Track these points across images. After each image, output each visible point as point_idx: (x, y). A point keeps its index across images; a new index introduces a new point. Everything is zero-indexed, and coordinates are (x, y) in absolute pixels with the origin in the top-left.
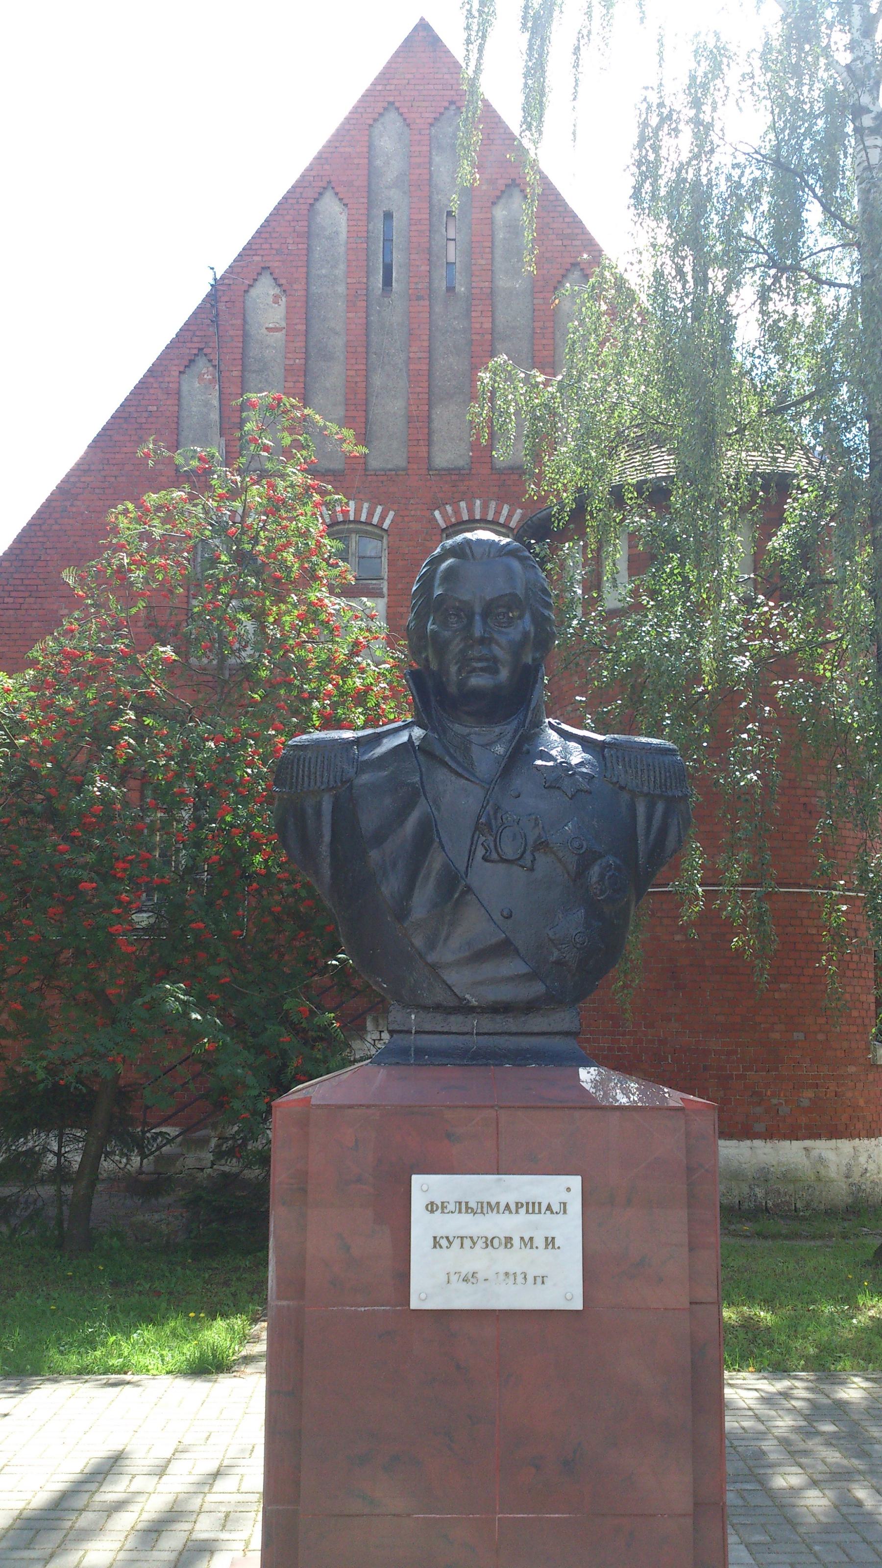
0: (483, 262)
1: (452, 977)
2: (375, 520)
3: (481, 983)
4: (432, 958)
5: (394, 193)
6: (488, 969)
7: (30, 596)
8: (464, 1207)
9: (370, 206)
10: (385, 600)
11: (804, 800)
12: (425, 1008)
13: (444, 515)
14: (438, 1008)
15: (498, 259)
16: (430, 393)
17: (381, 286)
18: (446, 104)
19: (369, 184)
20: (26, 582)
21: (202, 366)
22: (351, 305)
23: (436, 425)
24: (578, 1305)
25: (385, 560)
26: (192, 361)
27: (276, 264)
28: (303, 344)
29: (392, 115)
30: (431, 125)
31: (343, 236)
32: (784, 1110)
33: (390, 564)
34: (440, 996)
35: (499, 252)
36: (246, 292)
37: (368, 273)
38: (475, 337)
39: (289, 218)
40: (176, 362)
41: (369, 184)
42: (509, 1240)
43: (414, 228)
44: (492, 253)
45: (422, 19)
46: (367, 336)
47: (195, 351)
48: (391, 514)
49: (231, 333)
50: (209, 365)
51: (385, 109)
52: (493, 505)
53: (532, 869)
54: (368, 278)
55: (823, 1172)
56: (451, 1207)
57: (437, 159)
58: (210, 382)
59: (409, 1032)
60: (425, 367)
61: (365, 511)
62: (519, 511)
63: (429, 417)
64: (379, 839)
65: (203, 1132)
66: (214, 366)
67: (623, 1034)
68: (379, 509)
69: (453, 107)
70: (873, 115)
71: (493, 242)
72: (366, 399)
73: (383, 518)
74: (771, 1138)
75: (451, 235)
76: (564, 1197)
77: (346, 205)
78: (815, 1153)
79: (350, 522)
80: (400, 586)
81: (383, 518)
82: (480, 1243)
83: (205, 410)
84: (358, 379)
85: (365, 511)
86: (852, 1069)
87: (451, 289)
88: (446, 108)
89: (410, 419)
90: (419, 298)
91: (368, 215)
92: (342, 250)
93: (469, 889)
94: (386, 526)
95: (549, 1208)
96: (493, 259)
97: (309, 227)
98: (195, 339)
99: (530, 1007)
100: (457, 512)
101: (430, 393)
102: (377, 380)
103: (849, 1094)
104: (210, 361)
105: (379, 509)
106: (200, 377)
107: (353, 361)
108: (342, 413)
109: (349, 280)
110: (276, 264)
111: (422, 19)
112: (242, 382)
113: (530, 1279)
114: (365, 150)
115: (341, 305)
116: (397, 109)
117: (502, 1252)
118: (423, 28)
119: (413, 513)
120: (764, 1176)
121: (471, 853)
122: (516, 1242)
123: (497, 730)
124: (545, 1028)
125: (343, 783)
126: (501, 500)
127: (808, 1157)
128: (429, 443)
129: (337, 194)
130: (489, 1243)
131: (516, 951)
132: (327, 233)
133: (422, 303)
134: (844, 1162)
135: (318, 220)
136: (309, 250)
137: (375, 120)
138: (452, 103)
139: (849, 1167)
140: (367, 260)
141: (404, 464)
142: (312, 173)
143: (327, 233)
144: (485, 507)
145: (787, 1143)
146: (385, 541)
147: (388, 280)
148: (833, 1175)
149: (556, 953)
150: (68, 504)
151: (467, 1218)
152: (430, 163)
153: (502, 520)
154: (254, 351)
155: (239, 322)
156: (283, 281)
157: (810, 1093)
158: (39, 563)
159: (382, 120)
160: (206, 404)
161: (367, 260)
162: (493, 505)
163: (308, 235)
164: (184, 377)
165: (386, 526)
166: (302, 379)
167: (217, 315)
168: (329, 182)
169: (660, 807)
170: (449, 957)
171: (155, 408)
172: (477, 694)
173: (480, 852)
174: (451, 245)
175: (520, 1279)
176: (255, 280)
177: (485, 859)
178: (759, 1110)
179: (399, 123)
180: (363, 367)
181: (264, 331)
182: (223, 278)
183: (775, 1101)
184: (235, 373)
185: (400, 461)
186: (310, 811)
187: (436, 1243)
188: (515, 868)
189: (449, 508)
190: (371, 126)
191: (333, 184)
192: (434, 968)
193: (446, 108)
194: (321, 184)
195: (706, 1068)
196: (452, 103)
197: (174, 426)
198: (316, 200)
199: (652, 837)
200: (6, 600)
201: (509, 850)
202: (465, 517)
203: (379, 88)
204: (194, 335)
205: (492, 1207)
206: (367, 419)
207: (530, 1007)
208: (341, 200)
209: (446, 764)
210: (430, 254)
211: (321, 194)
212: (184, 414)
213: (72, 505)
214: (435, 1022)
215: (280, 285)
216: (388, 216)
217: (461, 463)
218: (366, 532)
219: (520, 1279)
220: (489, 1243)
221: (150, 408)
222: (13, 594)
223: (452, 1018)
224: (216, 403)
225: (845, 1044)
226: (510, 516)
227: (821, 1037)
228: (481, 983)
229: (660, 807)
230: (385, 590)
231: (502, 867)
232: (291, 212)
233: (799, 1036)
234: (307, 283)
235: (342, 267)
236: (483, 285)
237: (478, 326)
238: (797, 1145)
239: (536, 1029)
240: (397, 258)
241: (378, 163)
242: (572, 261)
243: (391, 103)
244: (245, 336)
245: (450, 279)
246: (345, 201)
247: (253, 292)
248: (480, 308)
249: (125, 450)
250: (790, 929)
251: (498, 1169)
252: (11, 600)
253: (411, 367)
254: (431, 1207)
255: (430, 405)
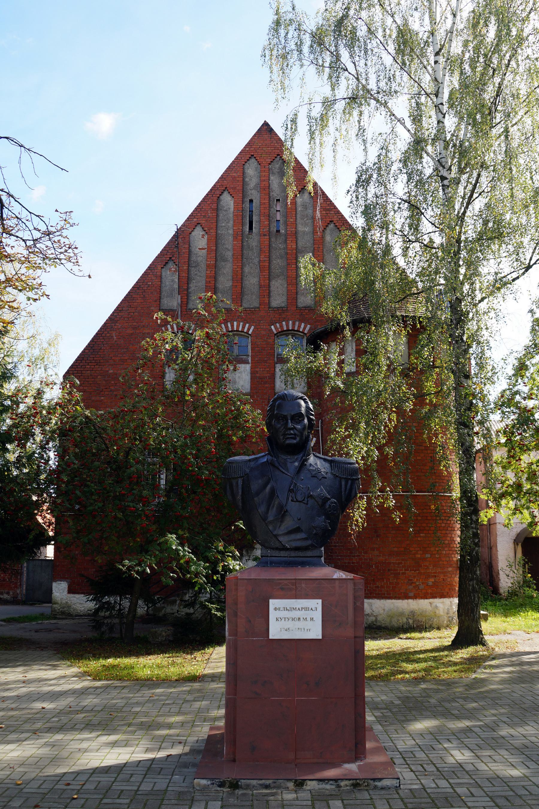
0: (292, 220)
1: (281, 539)
2: (245, 330)
3: (291, 541)
4: (275, 533)
5: (254, 192)
6: (293, 536)
7: (97, 365)
8: (286, 609)
9: (243, 197)
10: (250, 365)
11: (431, 455)
12: (273, 549)
13: (276, 328)
14: (277, 549)
15: (298, 219)
16: (269, 275)
17: (248, 230)
18: (276, 156)
19: (243, 189)
20: (95, 359)
21: (171, 265)
22: (235, 238)
23: (272, 288)
24: (320, 637)
25: (250, 347)
26: (166, 263)
27: (203, 222)
28: (214, 255)
29: (253, 160)
30: (269, 164)
31: (232, 210)
32: (422, 587)
33: (252, 349)
34: (278, 545)
35: (298, 216)
36: (190, 233)
37: (243, 225)
38: (288, 251)
39: (209, 202)
40: (160, 263)
41: (243, 189)
42: (299, 619)
43: (262, 206)
44: (296, 216)
45: (265, 121)
46: (242, 251)
47: (168, 259)
48: (253, 327)
49: (184, 251)
50: (174, 264)
51: (250, 158)
52: (297, 323)
53: (307, 504)
54: (242, 227)
55: (437, 612)
56: (282, 609)
57: (272, 178)
58: (174, 271)
59: (268, 556)
60: (267, 264)
61: (241, 326)
62: (309, 326)
63: (269, 285)
64: (258, 494)
65: (173, 598)
66: (176, 265)
67: (354, 556)
68: (247, 325)
69: (279, 157)
70: (448, 180)
71: (296, 212)
72: (242, 278)
73: (249, 329)
74: (416, 599)
75: (278, 209)
76: (317, 606)
77: (233, 197)
78: (434, 605)
79: (235, 331)
80: (256, 359)
81: (249, 329)
82: (291, 620)
83: (172, 283)
84: (238, 270)
85: (241, 326)
86: (450, 569)
87: (278, 231)
88: (276, 157)
89: (260, 286)
90: (265, 235)
91: (243, 201)
92: (231, 215)
93: (287, 511)
94: (250, 332)
95: (312, 609)
96: (296, 219)
97: (217, 206)
98: (168, 254)
99: (306, 548)
100: (281, 326)
101: (269, 275)
102: (247, 269)
103: (449, 580)
104: (175, 263)
105: (247, 325)
106: (170, 270)
107: (236, 262)
108: (231, 284)
109: (234, 228)
110: (203, 222)
111: (265, 121)
112: (188, 271)
113: (306, 630)
114: (242, 174)
115: (231, 238)
116: (255, 157)
117: (297, 622)
118: (266, 125)
119: (262, 327)
120: (413, 613)
121: (288, 499)
122: (302, 619)
123: (296, 457)
124: (311, 555)
125: (245, 475)
126: (301, 321)
127: (431, 606)
128: (269, 296)
129: (229, 192)
130: (293, 619)
131: (302, 531)
132: (225, 209)
133: (266, 237)
134: (446, 608)
135: (221, 203)
136: (217, 216)
137: (246, 162)
138: (278, 155)
139: (448, 610)
140: (242, 220)
141: (258, 305)
142: (219, 184)
143: (225, 209)
144: (294, 324)
145: (423, 600)
146: (250, 339)
147: (251, 228)
148: (442, 613)
149: (315, 531)
150: (113, 324)
151: (286, 612)
152: (269, 180)
153: (301, 330)
154: (193, 258)
155: (187, 246)
156: (206, 229)
157: (432, 580)
158: (101, 351)
159: (248, 162)
160: (173, 281)
161: (242, 220)
162: (297, 323)
163: (217, 210)
164: (164, 269)
165: (250, 332)
166: (214, 270)
167: (178, 244)
168: (226, 188)
169: (350, 482)
170: (281, 533)
171: (151, 283)
172: (290, 445)
173: (290, 499)
174: (278, 213)
175: (303, 630)
176: (194, 229)
177: (292, 501)
178: (411, 587)
179: (256, 163)
180: (241, 264)
181: (198, 250)
182: (180, 228)
183: (417, 583)
184: (185, 268)
185: (256, 304)
186: (234, 484)
187: (277, 620)
188: (302, 504)
189: (278, 325)
190: (244, 165)
191: (228, 189)
192: (276, 536)
193: (276, 157)
194: (223, 189)
195: (389, 570)
196: (278, 155)
197: (159, 290)
198: (220, 195)
199: (347, 492)
200: (87, 366)
201: (299, 499)
202: (285, 329)
203: (247, 149)
204: (168, 252)
205: (295, 609)
206: (242, 286)
207: (306, 548)
208: (231, 195)
209: (279, 469)
210: (269, 217)
211: (222, 193)
212: (163, 285)
213: (115, 325)
214: (276, 553)
215: (205, 231)
216: (251, 201)
217: (283, 305)
218: (242, 335)
219: (303, 630)
220: (293, 619)
221: (148, 283)
222: (90, 364)
223: (282, 552)
224: (177, 280)
225: (447, 559)
226: (304, 328)
227: (437, 556)
228: (291, 541)
229: (350, 482)
230: (250, 361)
231: (297, 503)
232: (210, 200)
233: (428, 556)
234: (216, 230)
235: (232, 222)
236: (292, 230)
237: (290, 247)
238: (427, 601)
239: (309, 555)
240: (255, 218)
241: (247, 179)
242: (330, 220)
243: (253, 155)
244: (190, 252)
245: (278, 226)
246: (233, 195)
247: (193, 233)
248: (291, 239)
249: (137, 301)
250: (425, 511)
251: (296, 597)
252: (89, 367)
253: (261, 264)
254: (276, 609)
255: (270, 280)
